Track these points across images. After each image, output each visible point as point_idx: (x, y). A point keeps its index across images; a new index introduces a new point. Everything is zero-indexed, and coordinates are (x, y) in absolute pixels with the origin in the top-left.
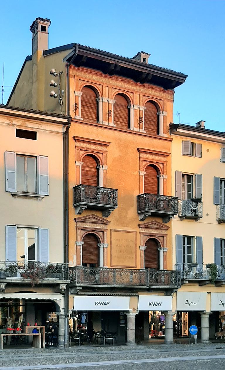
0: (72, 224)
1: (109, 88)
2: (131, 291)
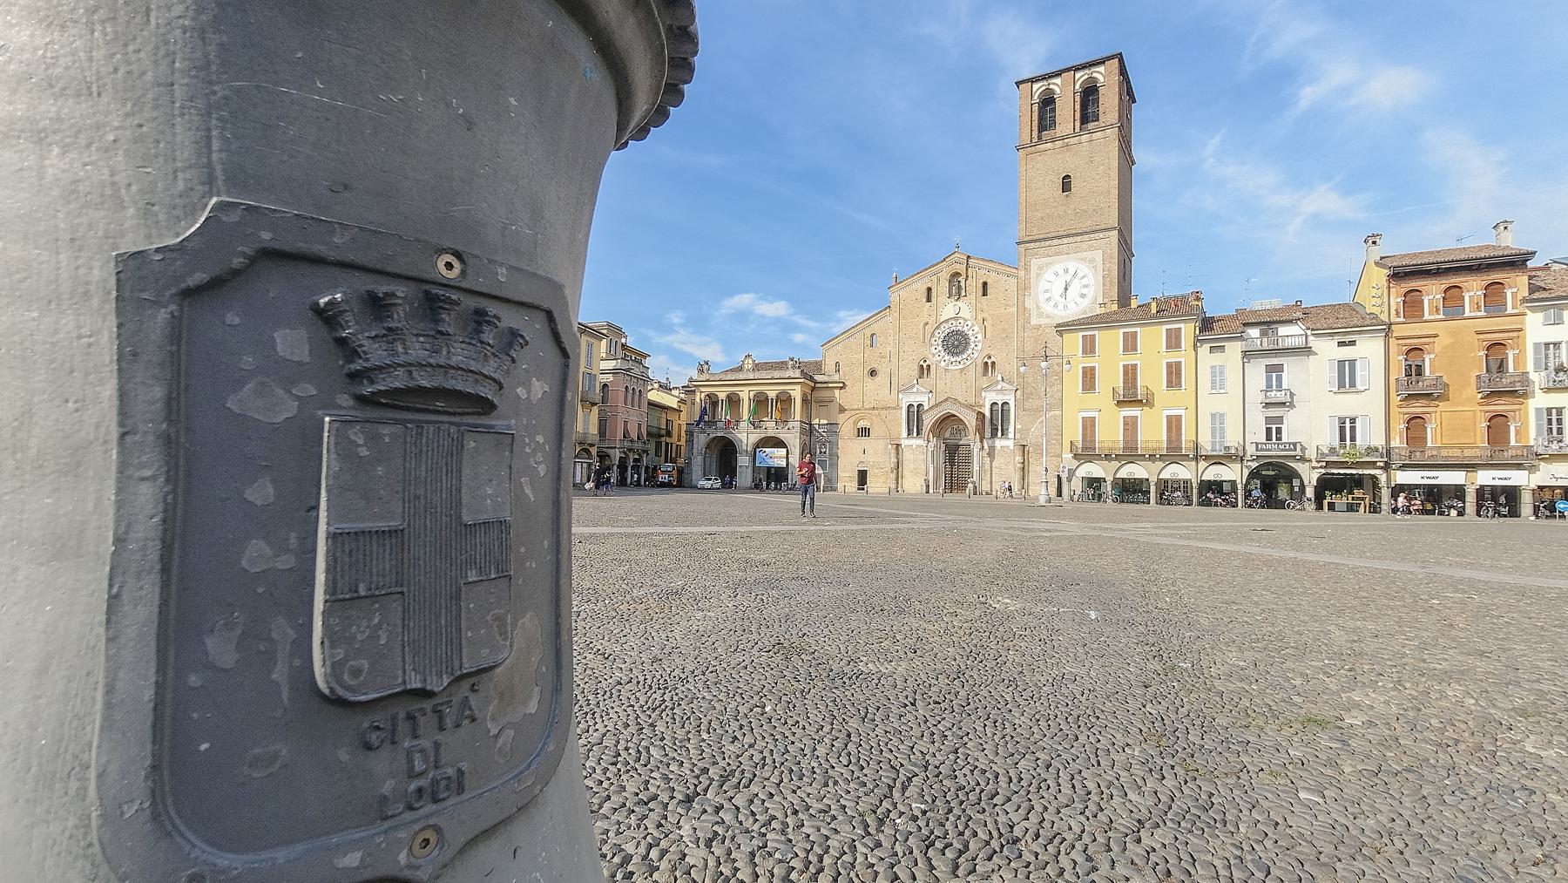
0: (1394, 410)
1: (1432, 292)
2: (1470, 467)
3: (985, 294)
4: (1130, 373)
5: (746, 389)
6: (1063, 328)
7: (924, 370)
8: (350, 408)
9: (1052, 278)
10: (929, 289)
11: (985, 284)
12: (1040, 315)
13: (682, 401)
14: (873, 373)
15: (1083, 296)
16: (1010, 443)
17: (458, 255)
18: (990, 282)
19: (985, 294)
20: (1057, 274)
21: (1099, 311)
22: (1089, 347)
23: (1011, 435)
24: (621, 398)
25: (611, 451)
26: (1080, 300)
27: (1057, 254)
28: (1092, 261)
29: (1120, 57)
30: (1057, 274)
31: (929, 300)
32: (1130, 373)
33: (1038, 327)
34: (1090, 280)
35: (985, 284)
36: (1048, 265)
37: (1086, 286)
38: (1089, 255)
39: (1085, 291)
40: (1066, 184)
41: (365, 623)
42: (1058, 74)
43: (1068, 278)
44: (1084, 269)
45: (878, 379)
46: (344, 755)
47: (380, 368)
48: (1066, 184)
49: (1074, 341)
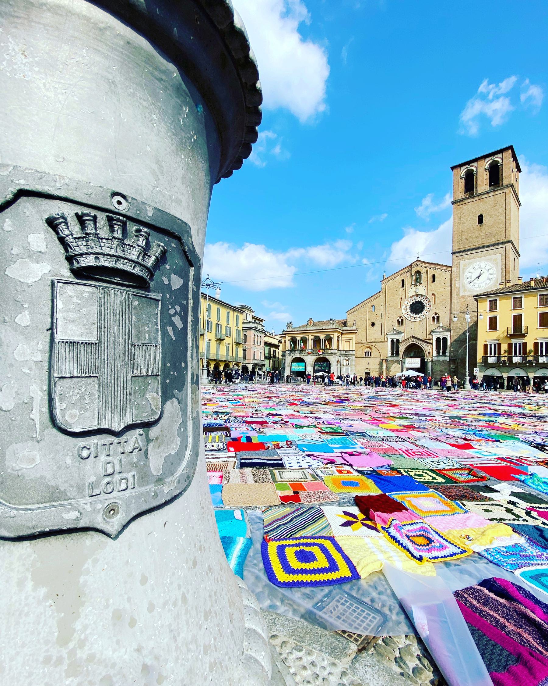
3: (434, 281)
4: (518, 320)
5: (310, 335)
6: (477, 298)
7: (401, 322)
8: (69, 277)
9: (472, 270)
10: (403, 281)
11: (434, 276)
12: (465, 290)
13: (280, 342)
14: (373, 324)
15: (490, 279)
16: (448, 359)
17: (124, 197)
18: (436, 275)
19: (434, 281)
20: (474, 269)
21: (499, 287)
22: (493, 306)
23: (448, 354)
24: (252, 339)
25: (248, 365)
26: (488, 282)
27: (475, 258)
28: (495, 260)
29: (511, 148)
30: (474, 269)
31: (403, 286)
32: (518, 320)
33: (463, 297)
34: (494, 271)
35: (434, 276)
36: (469, 264)
37: (491, 274)
38: (494, 257)
39: (491, 276)
40: (481, 219)
41: (76, 391)
42: (476, 160)
43: (476, 281)
44: (490, 265)
45: (375, 327)
46: (69, 461)
47: (81, 255)
48: (481, 219)
49: (484, 306)
